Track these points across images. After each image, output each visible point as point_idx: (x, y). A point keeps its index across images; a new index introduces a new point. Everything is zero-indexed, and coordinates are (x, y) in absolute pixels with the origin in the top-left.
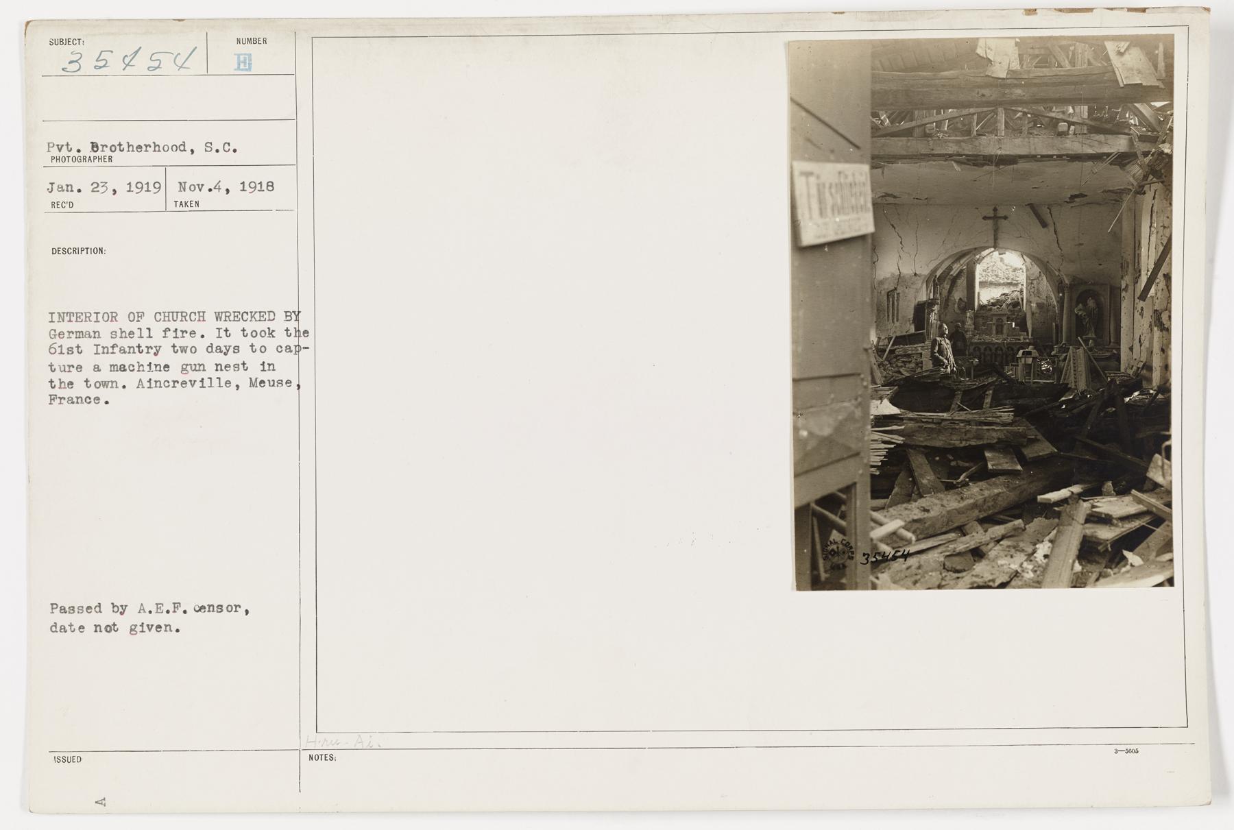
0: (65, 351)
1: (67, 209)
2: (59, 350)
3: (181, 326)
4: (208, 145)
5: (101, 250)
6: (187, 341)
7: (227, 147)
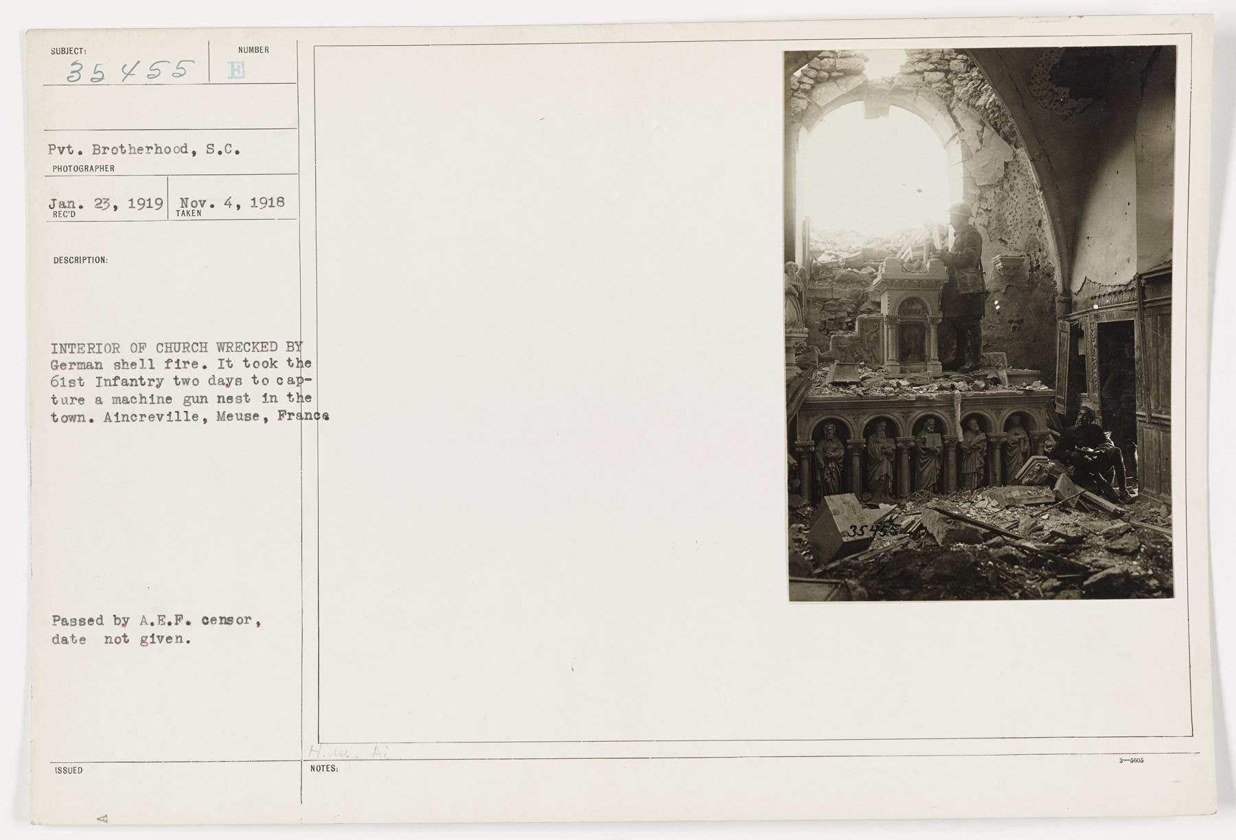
0: (67, 383)
1: (69, 218)
2: (61, 383)
3: (183, 357)
5: (103, 260)
6: (188, 373)
7: (228, 148)
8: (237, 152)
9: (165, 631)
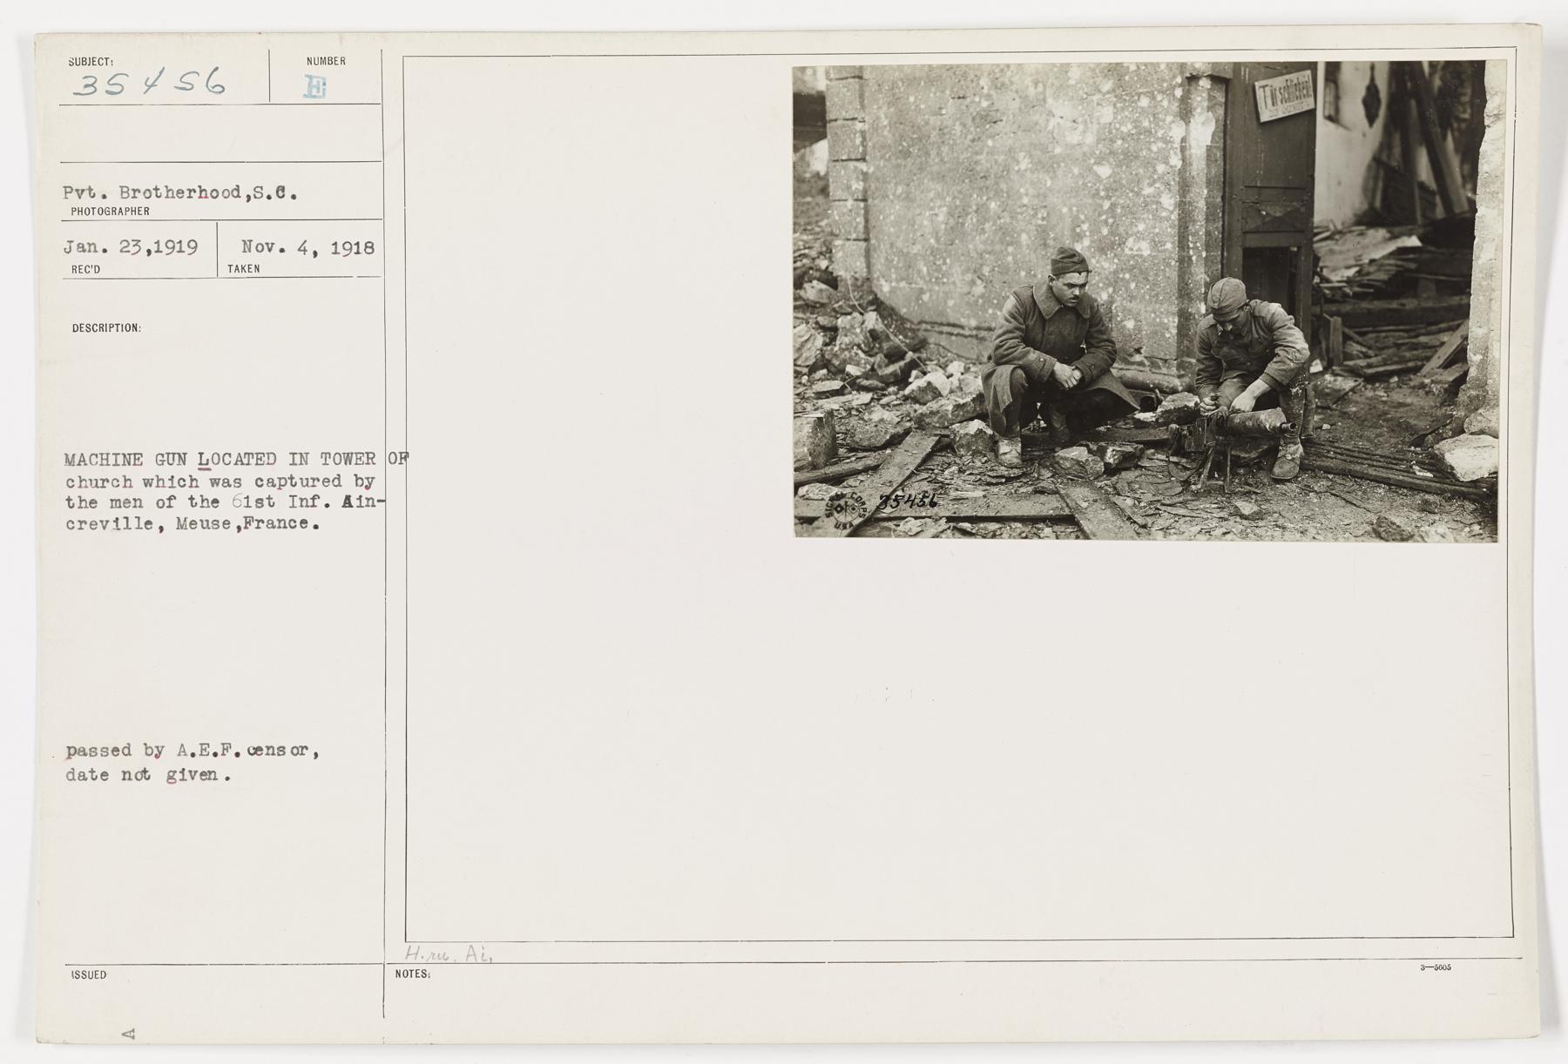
5: (135, 327)
8: (294, 197)
9: (200, 768)
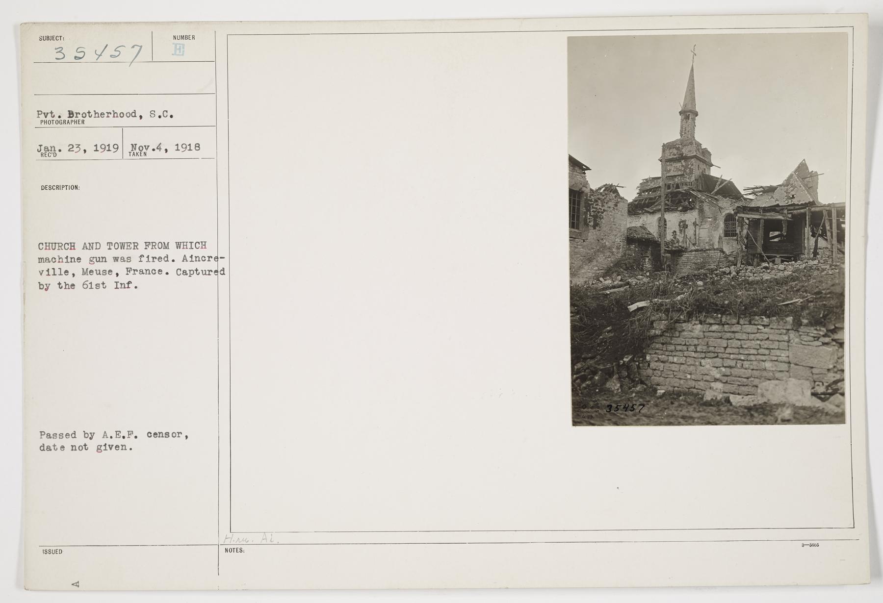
4: (152, 113)
5: (76, 187)
8: (171, 116)
